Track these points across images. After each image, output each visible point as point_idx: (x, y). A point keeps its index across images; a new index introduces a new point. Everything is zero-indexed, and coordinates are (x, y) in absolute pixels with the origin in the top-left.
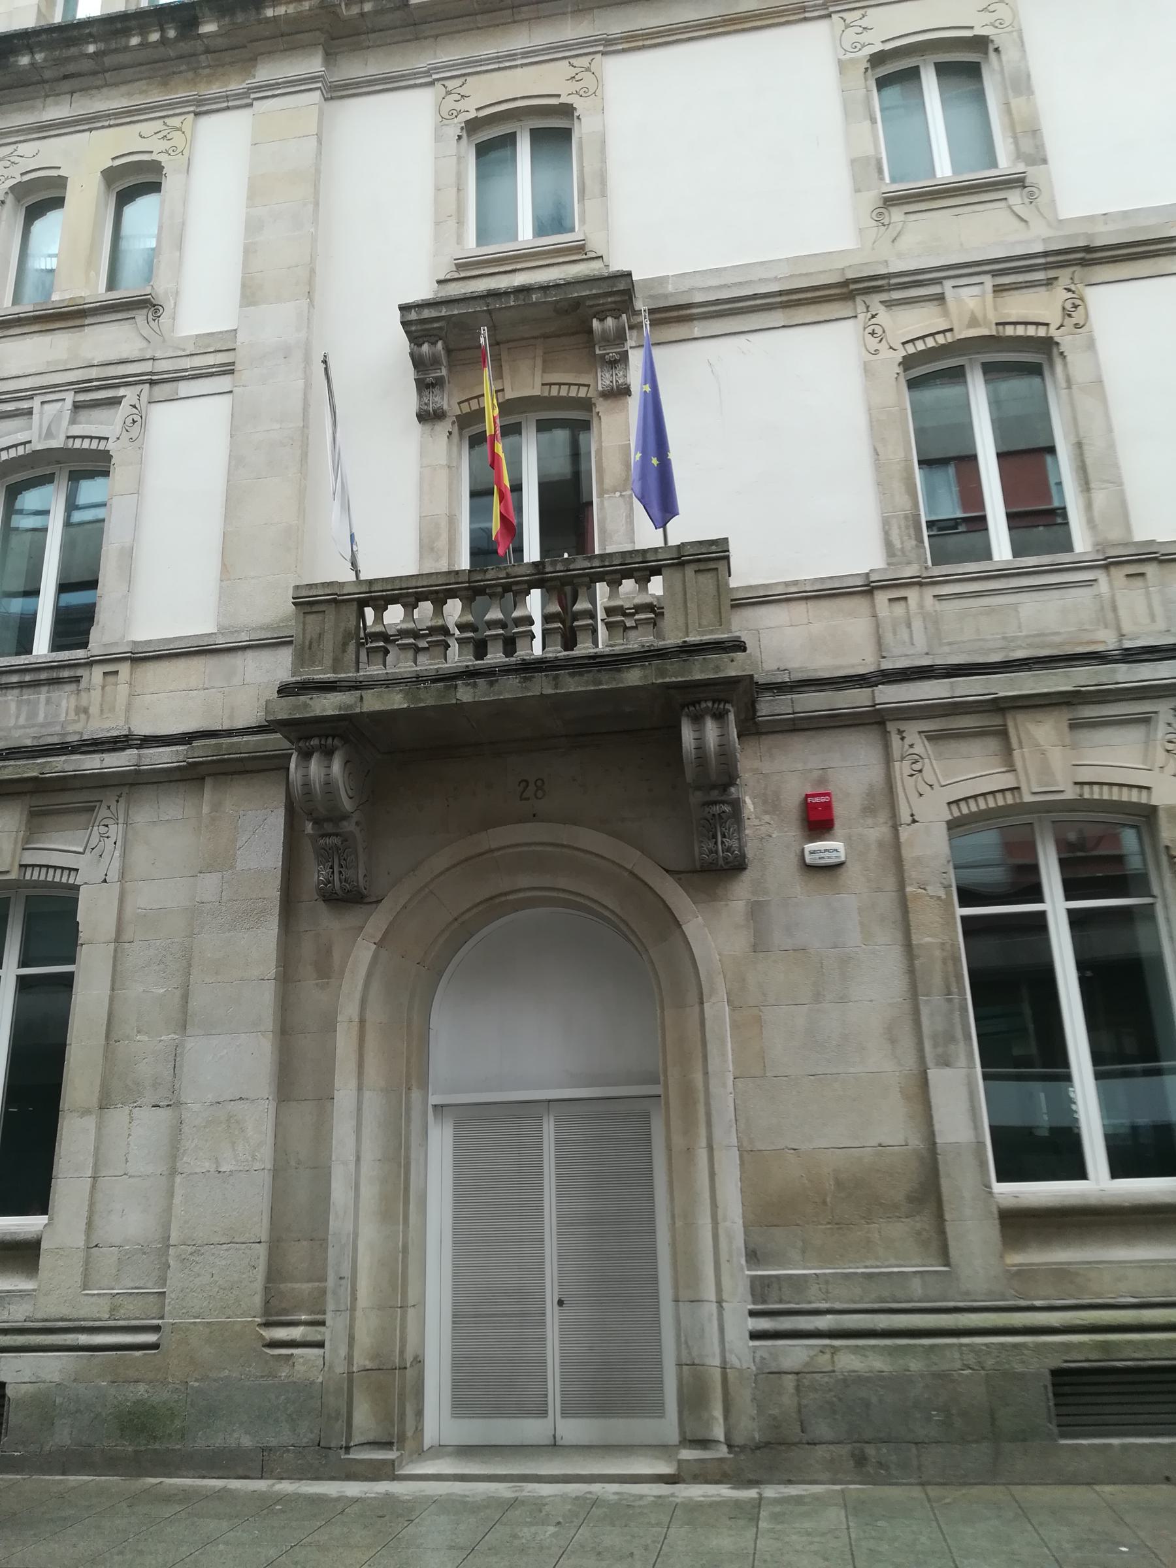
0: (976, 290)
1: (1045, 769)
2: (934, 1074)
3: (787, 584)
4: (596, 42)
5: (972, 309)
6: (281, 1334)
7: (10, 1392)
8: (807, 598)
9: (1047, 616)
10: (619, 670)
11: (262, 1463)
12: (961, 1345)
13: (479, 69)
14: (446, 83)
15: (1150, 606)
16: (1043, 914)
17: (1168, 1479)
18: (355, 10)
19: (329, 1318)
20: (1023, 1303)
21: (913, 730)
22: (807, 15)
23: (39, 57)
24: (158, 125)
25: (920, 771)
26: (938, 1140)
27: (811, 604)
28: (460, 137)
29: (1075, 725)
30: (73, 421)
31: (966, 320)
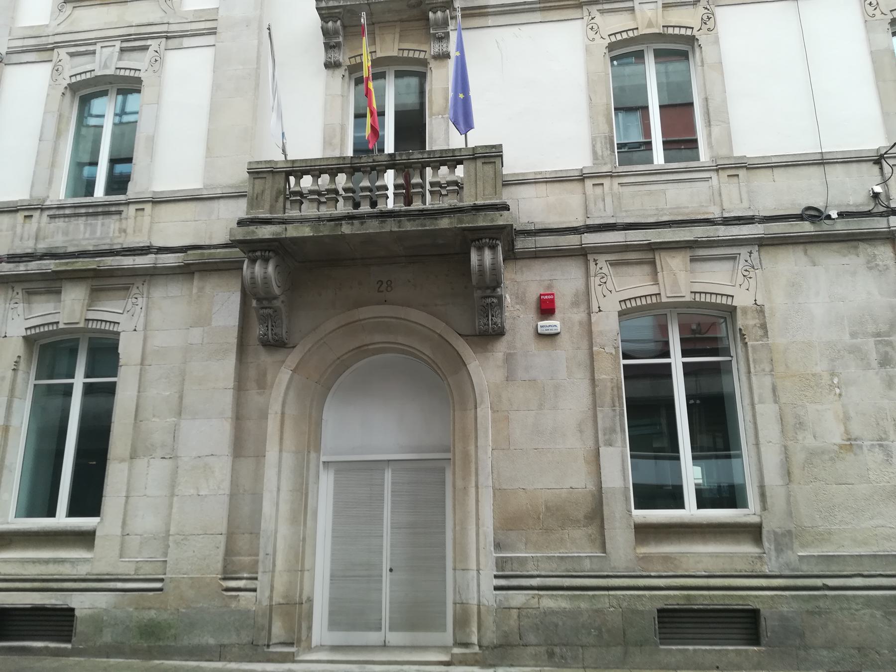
1: (675, 283)
3: (535, 173)
7: (77, 613)
8: (546, 182)
10: (436, 219)
16: (669, 365)
17: (718, 667)
19: (260, 576)
20: (644, 574)
21: (602, 259)
30: (120, 59)
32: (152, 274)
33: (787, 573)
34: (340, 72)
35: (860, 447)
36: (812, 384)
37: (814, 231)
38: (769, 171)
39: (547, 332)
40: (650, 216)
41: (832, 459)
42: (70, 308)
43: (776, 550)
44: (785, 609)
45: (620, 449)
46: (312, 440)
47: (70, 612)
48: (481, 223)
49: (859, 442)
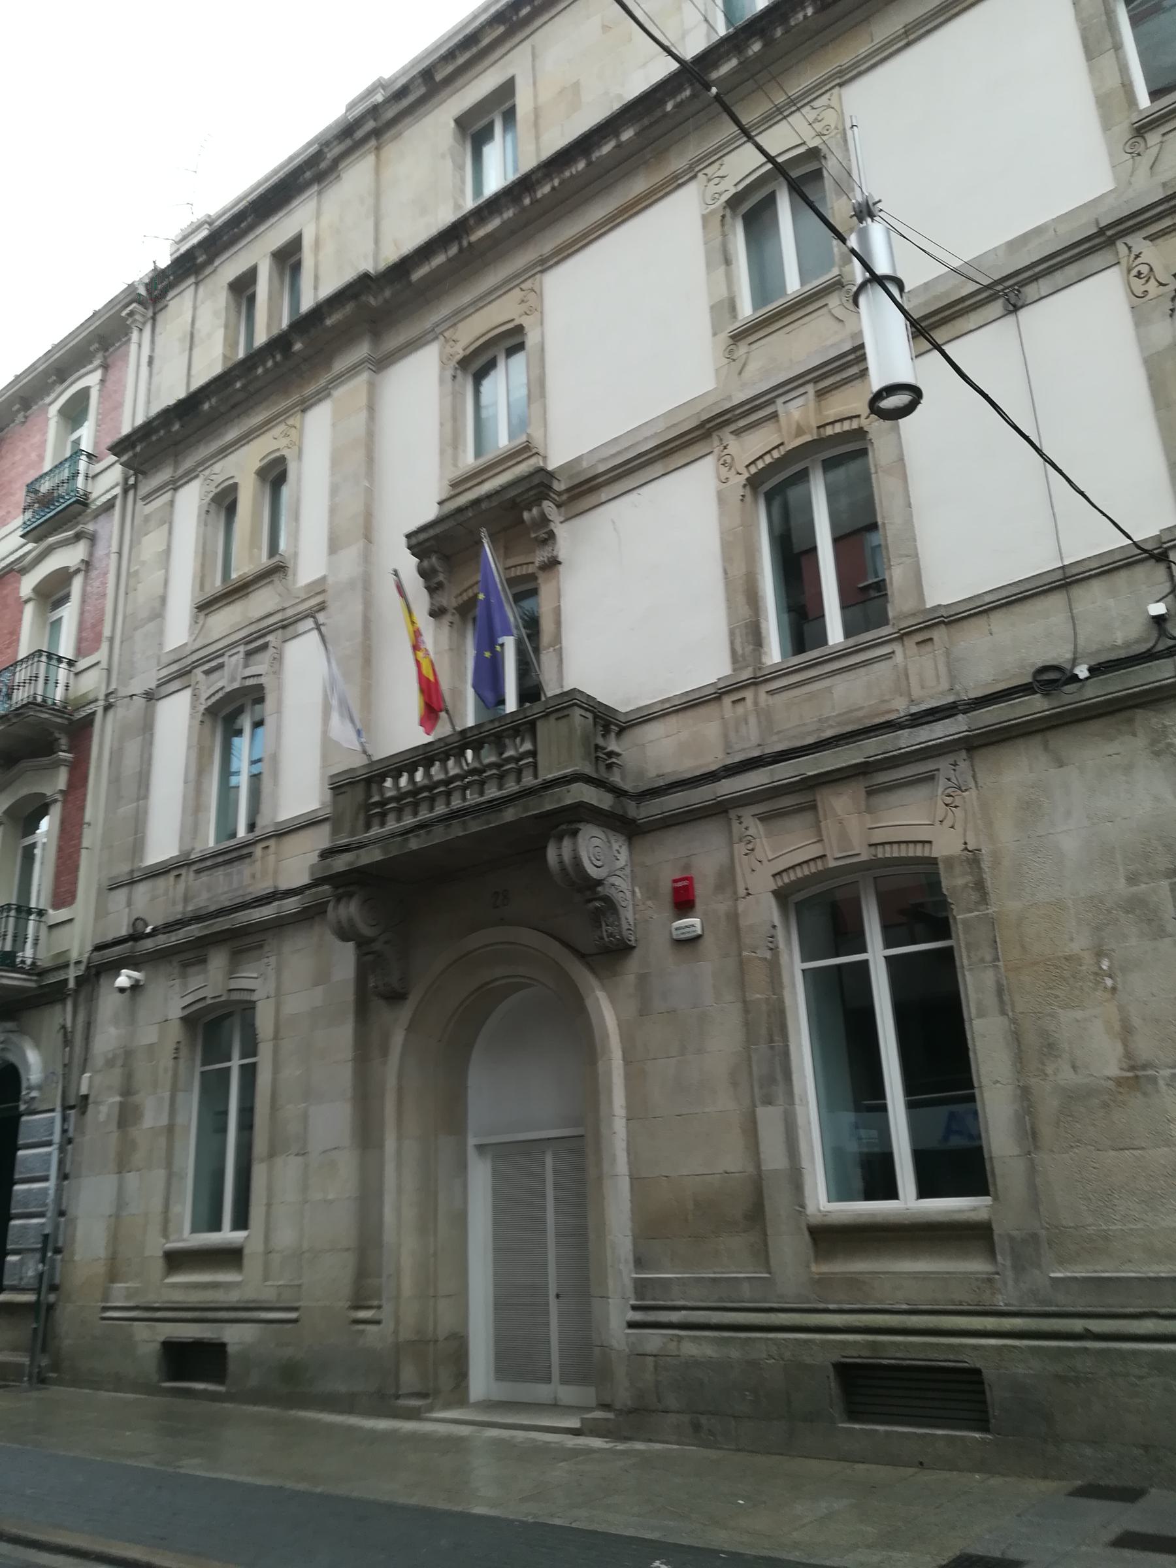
0: (800, 401)
1: (844, 837)
2: (761, 1111)
3: (662, 702)
4: (535, 265)
5: (799, 415)
6: (362, 1314)
7: (230, 1349)
8: (677, 711)
9: (852, 695)
10: (500, 811)
11: (347, 1404)
12: (768, 1339)
13: (890, 51)
14: (705, 171)
15: (936, 668)
16: (866, 962)
17: (921, 1464)
18: (380, 299)
19: (384, 1302)
20: (821, 1306)
21: (747, 813)
22: (680, 181)
23: (213, 401)
24: (282, 427)
25: (753, 850)
26: (763, 1168)
27: (681, 715)
28: (454, 377)
29: (871, 792)
30: (246, 666)
31: (793, 432)
32: (279, 925)
33: (1033, 1307)
34: (447, 619)
35: (1153, 1080)
36: (1066, 974)
37: (1057, 708)
38: (981, 621)
39: (683, 936)
40: (809, 733)
41: (1105, 1105)
42: (212, 981)
43: (1014, 1267)
44: (1020, 1370)
45: (781, 1109)
46: (451, 1116)
47: (222, 1347)
48: (548, 807)
49: (1150, 1072)
